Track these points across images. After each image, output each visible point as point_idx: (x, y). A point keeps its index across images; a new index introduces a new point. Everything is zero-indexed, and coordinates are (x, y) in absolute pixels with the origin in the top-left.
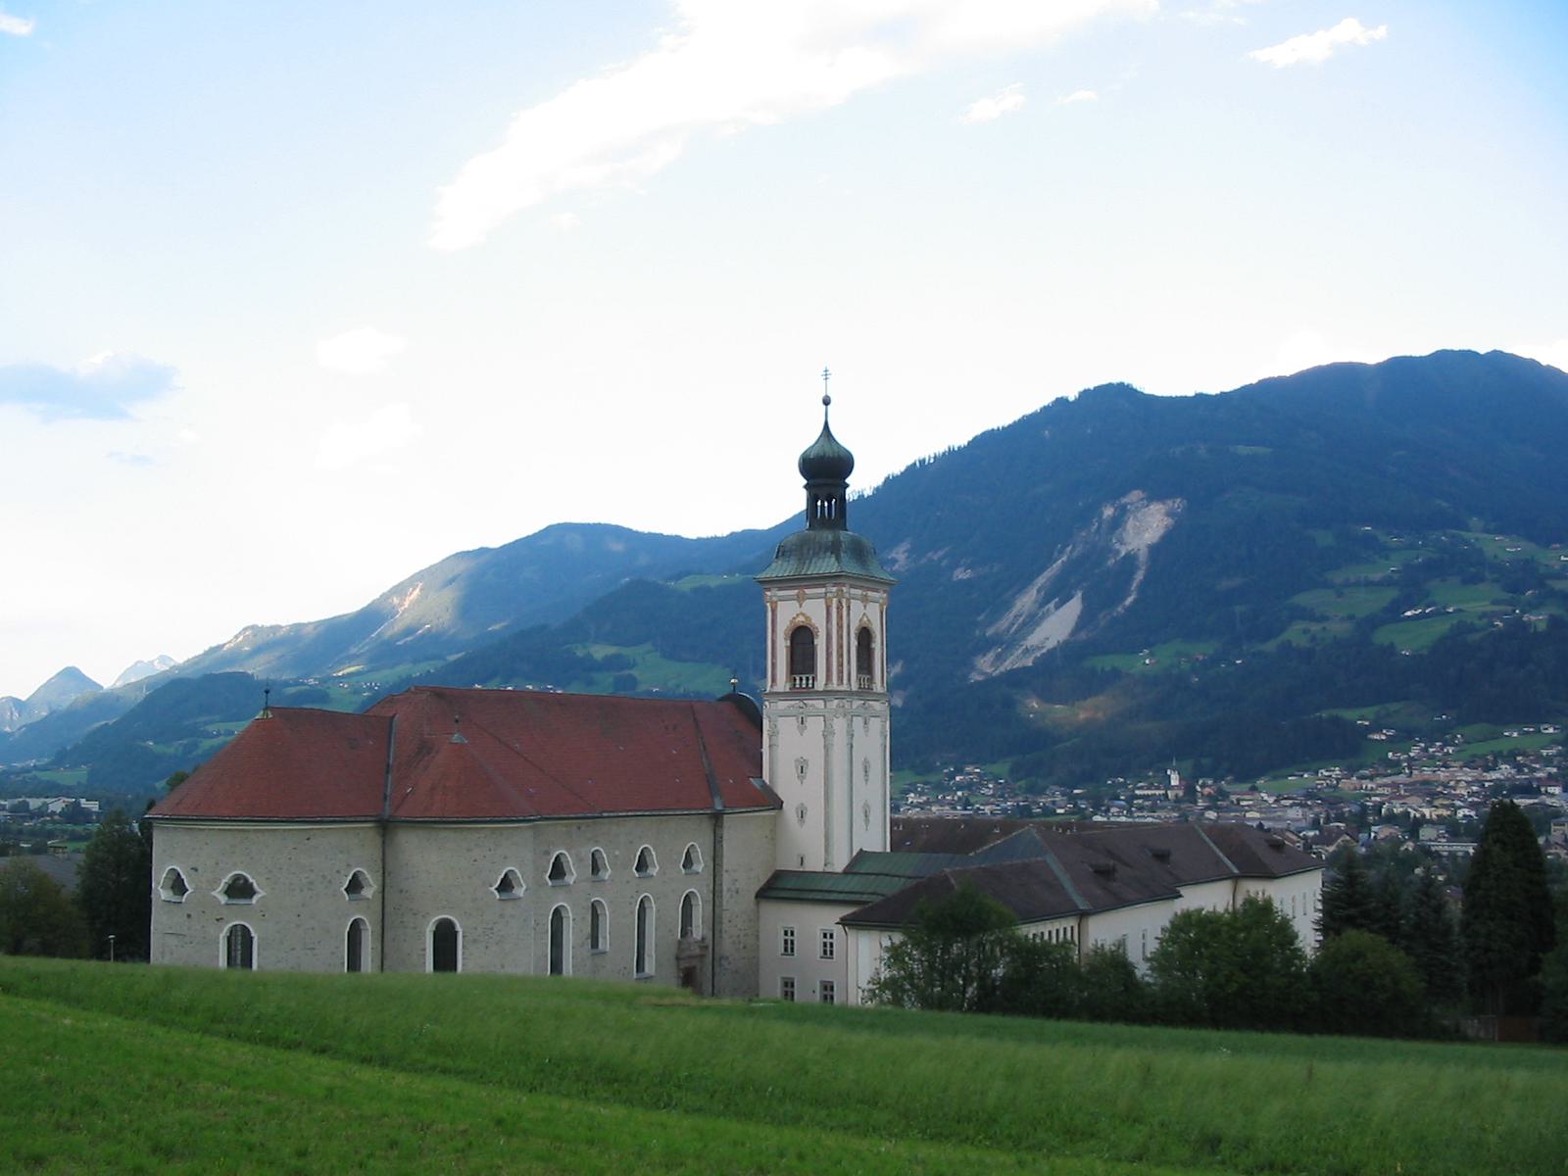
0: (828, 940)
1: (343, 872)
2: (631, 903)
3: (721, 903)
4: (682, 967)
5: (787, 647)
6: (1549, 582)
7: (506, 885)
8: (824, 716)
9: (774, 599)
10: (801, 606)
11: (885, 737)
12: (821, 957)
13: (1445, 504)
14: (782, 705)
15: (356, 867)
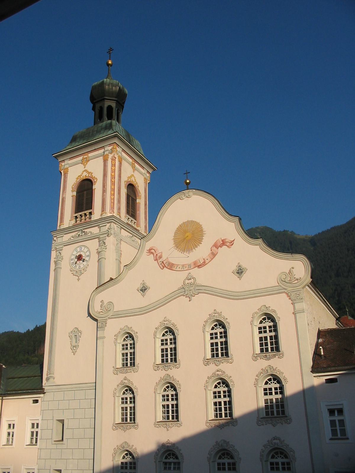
0: (35, 430)
9: (66, 166)
10: (85, 167)
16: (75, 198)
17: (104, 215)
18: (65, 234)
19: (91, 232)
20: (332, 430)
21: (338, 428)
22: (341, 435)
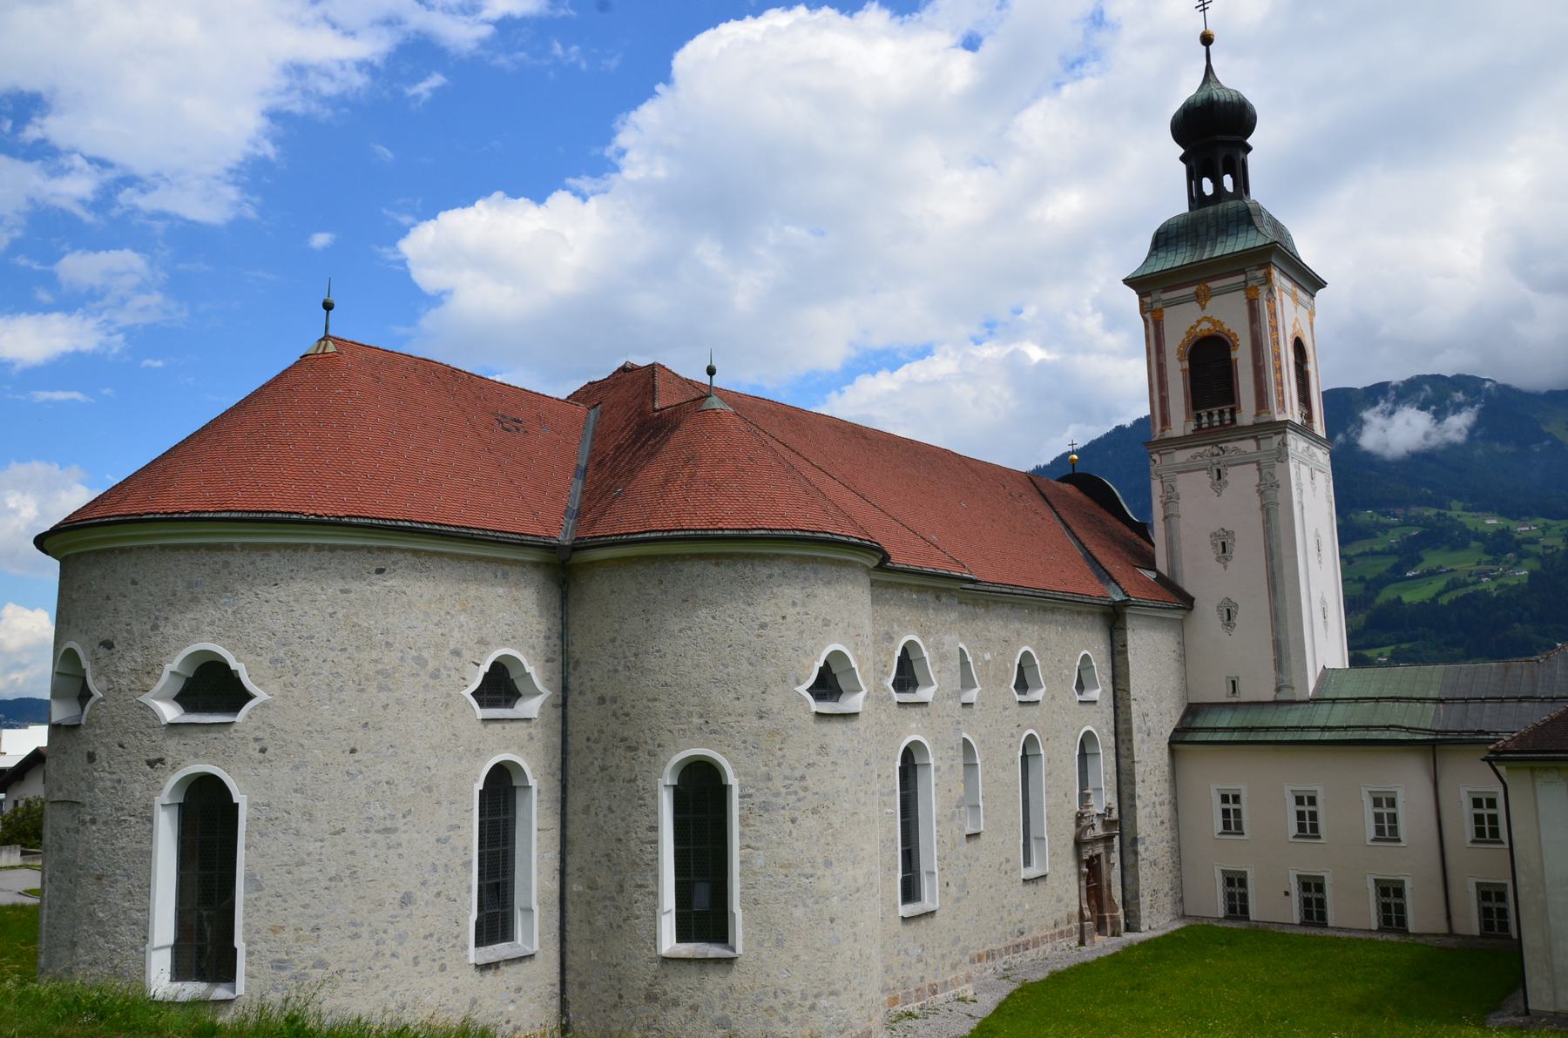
1: (467, 655)
2: (1010, 746)
3: (1130, 749)
4: (1086, 857)
5: (1183, 370)
6: (1525, 547)
7: (827, 684)
8: (1258, 463)
9: (1158, 306)
11: (1331, 502)
12: (1296, 837)
13: (1429, 492)
14: (1181, 456)
15: (498, 646)
16: (1188, 373)
17: (1265, 417)
18: (1177, 449)
19: (1236, 449)
20: (1477, 828)
21: (1307, 822)
22: (1236, 829)
